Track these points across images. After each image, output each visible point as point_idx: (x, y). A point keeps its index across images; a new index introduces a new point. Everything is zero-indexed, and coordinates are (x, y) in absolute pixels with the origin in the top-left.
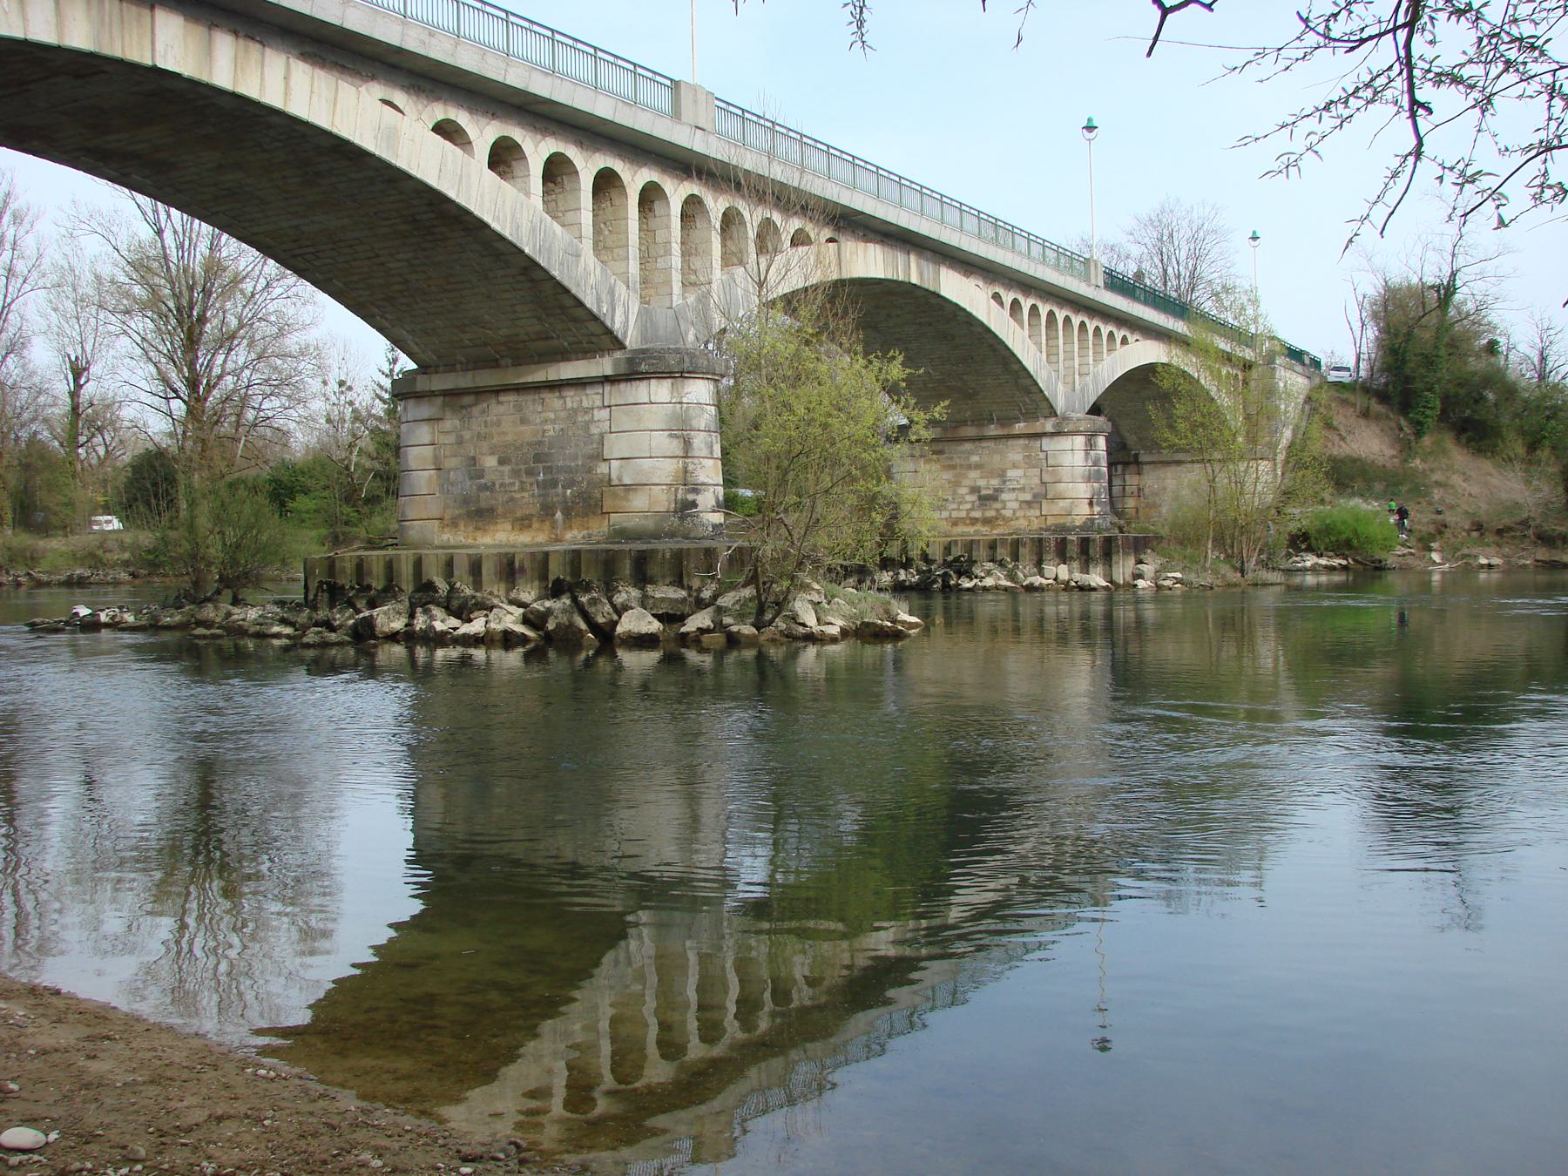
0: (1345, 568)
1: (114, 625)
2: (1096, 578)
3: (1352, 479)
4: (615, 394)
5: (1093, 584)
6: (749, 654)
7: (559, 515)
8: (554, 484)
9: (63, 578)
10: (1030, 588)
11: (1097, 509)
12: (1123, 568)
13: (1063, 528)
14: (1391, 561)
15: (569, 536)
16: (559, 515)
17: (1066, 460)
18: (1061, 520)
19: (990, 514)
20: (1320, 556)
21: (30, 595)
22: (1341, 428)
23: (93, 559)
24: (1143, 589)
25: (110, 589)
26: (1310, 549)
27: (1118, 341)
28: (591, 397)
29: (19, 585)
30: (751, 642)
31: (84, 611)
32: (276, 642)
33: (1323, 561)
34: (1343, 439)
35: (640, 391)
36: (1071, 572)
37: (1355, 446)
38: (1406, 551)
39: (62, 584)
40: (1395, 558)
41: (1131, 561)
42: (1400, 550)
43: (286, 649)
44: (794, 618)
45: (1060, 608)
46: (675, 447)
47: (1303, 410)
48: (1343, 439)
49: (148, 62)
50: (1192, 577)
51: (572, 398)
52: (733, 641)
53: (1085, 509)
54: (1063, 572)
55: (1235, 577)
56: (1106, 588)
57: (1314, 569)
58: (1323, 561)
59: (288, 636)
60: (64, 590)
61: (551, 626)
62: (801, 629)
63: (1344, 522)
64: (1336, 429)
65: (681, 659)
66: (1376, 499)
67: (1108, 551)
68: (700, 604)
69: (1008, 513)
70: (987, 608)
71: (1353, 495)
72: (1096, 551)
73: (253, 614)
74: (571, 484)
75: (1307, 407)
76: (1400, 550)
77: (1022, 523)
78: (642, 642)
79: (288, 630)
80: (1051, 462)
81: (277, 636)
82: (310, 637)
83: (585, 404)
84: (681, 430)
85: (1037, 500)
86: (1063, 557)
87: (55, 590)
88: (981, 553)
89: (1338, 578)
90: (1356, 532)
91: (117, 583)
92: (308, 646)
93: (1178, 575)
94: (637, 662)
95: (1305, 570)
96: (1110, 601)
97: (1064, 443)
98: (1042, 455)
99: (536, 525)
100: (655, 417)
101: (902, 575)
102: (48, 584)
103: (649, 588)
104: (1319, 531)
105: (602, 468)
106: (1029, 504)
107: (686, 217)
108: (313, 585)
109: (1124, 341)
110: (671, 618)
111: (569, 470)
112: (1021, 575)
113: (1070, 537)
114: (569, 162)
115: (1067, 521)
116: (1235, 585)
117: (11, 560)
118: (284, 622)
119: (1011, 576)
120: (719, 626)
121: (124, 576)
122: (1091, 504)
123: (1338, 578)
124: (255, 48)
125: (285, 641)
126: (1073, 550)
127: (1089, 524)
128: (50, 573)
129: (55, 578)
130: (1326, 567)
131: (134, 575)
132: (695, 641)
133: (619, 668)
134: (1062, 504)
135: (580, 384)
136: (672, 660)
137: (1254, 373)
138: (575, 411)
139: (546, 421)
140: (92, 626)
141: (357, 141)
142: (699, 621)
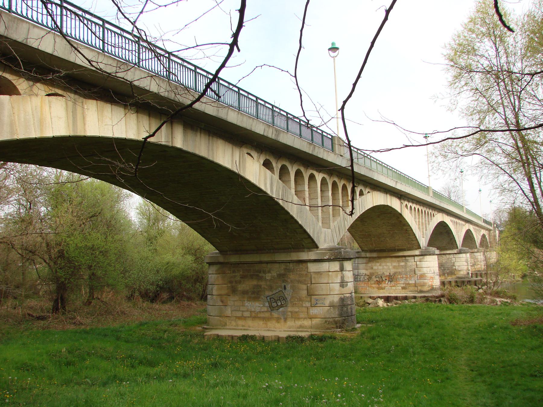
4: (456, 256)
7: (446, 275)
8: (445, 270)
15: (448, 278)
16: (446, 275)
17: (479, 257)
18: (479, 269)
28: (452, 256)
35: (461, 255)
46: (466, 264)
49: (386, 204)
51: (448, 256)
74: (448, 270)
80: (476, 258)
83: (450, 257)
84: (467, 261)
97: (478, 254)
98: (474, 256)
99: (442, 276)
100: (463, 259)
105: (454, 267)
107: (322, 184)
109: (361, 194)
111: (448, 268)
114: (301, 173)
115: (480, 269)
124: (80, 99)
135: (450, 254)
138: (448, 258)
139: (443, 260)
141: (396, 209)
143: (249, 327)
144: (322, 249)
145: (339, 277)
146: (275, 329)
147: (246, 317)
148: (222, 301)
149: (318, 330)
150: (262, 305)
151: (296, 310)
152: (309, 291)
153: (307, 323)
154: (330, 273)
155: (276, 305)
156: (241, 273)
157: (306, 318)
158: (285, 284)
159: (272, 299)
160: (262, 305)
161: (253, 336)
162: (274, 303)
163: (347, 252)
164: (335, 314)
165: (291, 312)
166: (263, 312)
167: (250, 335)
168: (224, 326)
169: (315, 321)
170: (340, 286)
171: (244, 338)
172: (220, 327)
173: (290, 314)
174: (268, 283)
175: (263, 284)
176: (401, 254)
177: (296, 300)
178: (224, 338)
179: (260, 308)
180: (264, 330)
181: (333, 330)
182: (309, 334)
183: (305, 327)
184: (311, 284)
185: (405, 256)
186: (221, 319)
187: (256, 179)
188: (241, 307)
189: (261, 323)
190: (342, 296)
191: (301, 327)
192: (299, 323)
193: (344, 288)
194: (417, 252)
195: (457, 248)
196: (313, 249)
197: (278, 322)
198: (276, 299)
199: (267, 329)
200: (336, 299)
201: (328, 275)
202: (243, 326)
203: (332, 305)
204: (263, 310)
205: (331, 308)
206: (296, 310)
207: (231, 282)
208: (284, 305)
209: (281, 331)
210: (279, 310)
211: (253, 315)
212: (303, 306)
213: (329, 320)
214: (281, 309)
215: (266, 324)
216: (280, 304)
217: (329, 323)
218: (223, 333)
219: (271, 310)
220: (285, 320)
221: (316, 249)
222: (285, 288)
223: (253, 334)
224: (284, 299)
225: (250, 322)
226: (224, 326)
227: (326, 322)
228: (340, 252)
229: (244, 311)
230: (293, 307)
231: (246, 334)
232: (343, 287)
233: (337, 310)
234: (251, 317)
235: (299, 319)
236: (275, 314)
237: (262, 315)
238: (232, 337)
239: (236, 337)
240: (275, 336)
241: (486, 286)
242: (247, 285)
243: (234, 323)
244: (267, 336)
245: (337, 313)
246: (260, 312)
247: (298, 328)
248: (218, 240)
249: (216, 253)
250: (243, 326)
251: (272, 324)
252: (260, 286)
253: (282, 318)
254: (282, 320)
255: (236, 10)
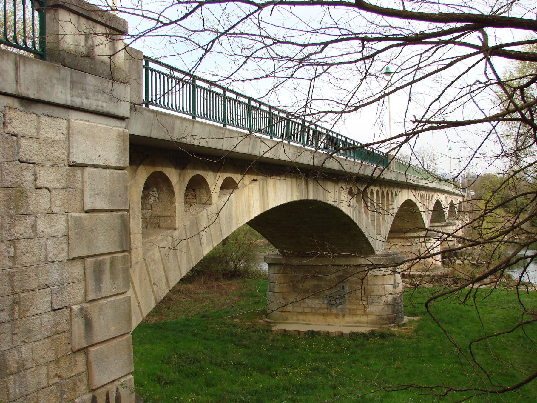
135: (438, 226)
143: (310, 321)
144: (378, 256)
145: (392, 280)
146: (334, 324)
147: (306, 313)
148: (284, 298)
149: (375, 326)
150: (322, 303)
151: (354, 307)
152: (366, 292)
153: (364, 319)
154: (385, 276)
155: (335, 303)
156: (302, 273)
157: (363, 315)
158: (344, 285)
159: (331, 298)
160: (322, 303)
161: (319, 332)
162: (333, 301)
163: (399, 258)
164: (388, 312)
165: (349, 309)
166: (323, 308)
167: (315, 330)
168: (286, 320)
169: (371, 318)
170: (393, 287)
171: (311, 334)
172: (282, 321)
173: (347, 310)
174: (328, 283)
175: (322, 283)
176: (407, 235)
177: (354, 299)
178: (291, 333)
179: (319, 305)
180: (325, 325)
181: (387, 325)
182: (369, 329)
183: (362, 323)
184: (368, 285)
185: (411, 237)
186: (283, 314)
187: (350, 212)
188: (302, 304)
189: (321, 318)
190: (395, 296)
191: (358, 322)
192: (356, 319)
193: (396, 289)
194: (423, 234)
195: (445, 221)
196: (370, 255)
197: (337, 318)
198: (335, 297)
199: (327, 324)
200: (390, 298)
201: (383, 278)
202: (304, 320)
203: (386, 304)
204: (322, 307)
205: (385, 307)
206: (354, 307)
207: (292, 281)
208: (343, 303)
209: (340, 326)
210: (338, 307)
211: (314, 310)
212: (360, 305)
213: (383, 316)
214: (340, 307)
215: (326, 319)
216: (338, 302)
217: (384, 319)
218: (290, 328)
219: (331, 307)
220: (344, 316)
221: (372, 255)
222: (343, 288)
223: (318, 330)
224: (342, 298)
225: (310, 317)
226: (285, 320)
227: (381, 318)
228: (394, 258)
229: (305, 307)
230: (351, 304)
231: (311, 329)
232: (395, 288)
233: (390, 308)
234: (311, 312)
235: (356, 315)
236: (334, 311)
237: (322, 311)
238: (299, 332)
239: (303, 333)
240: (338, 332)
241: (471, 257)
242: (309, 284)
243: (295, 318)
244: (332, 332)
245: (390, 311)
246: (320, 308)
247: (355, 323)
248: (284, 245)
249: (278, 255)
250: (304, 320)
251: (331, 319)
252: (320, 286)
253: (341, 314)
254: (341, 316)
255: (414, 115)
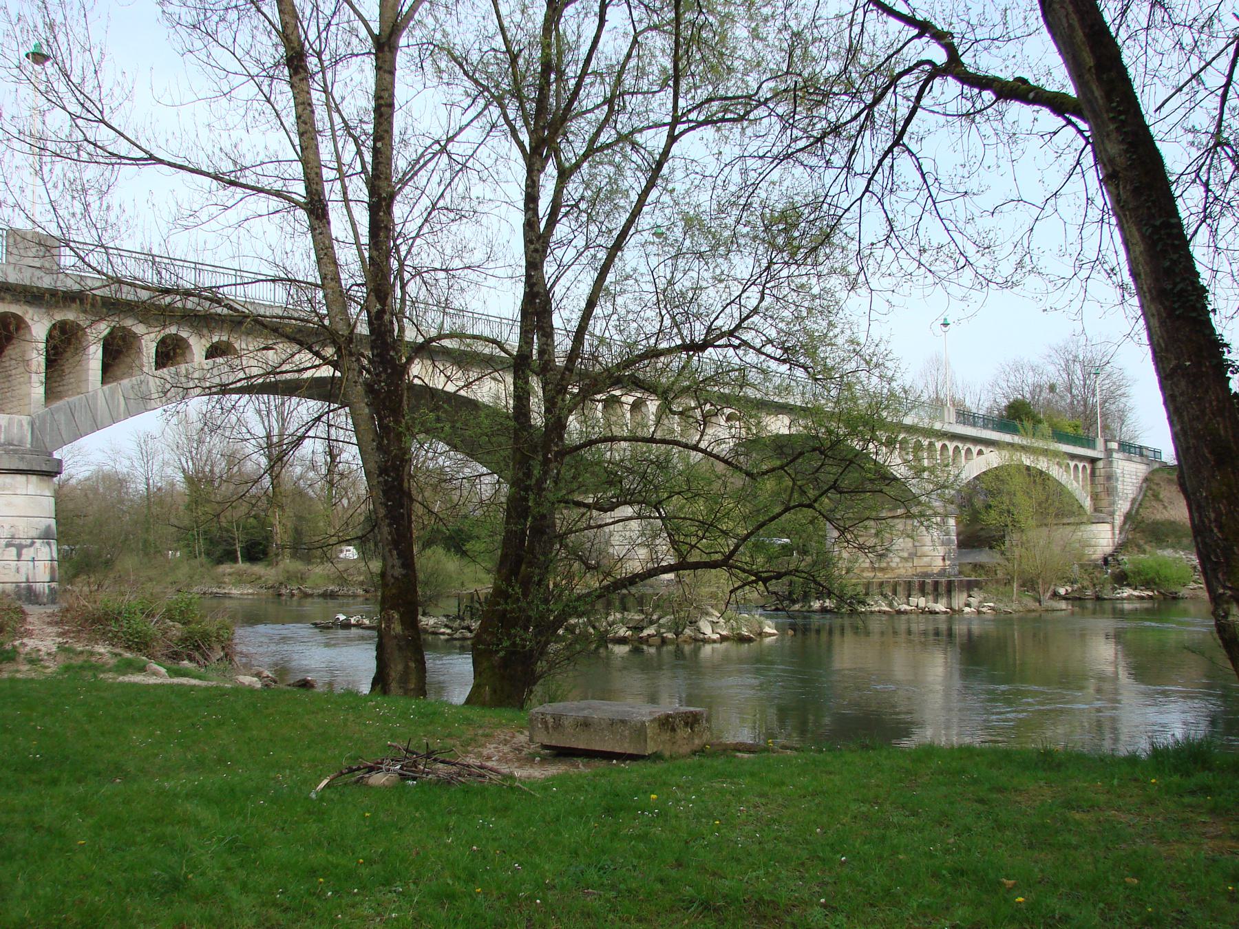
0: (1151, 597)
1: (359, 625)
2: (940, 607)
3: (1167, 536)
5: (937, 610)
6: (671, 648)
9: (321, 591)
10: (899, 612)
11: (948, 563)
12: (959, 600)
13: (926, 575)
14: (1183, 592)
18: (925, 570)
19: (884, 565)
20: (1136, 589)
21: (300, 604)
22: (1165, 500)
23: (342, 579)
24: (967, 613)
25: (351, 600)
26: (1128, 585)
27: (963, 452)
29: (293, 595)
30: (672, 642)
31: (342, 617)
32: (442, 637)
33: (1136, 593)
34: (1165, 507)
36: (927, 602)
37: (1172, 513)
38: (1196, 586)
39: (320, 596)
40: (1188, 592)
41: (965, 595)
42: (1192, 585)
43: (447, 640)
44: (698, 630)
45: (919, 625)
47: (1141, 488)
48: (1165, 507)
50: (1001, 606)
52: (664, 641)
53: (940, 563)
54: (922, 602)
55: (1033, 605)
56: (946, 613)
57: (1129, 598)
58: (1136, 593)
59: (448, 634)
60: (321, 600)
61: (577, 631)
62: (701, 636)
63: (1151, 567)
64: (1161, 501)
65: (642, 651)
66: (1183, 550)
67: (950, 589)
68: (651, 623)
69: (893, 565)
70: (875, 625)
71: (1167, 547)
72: (942, 589)
73: (432, 621)
75: (1144, 485)
76: (1192, 585)
77: (902, 571)
78: (622, 641)
79: (449, 631)
81: (443, 634)
82: (457, 635)
85: (913, 555)
86: (923, 592)
87: (316, 600)
88: (874, 589)
89: (1146, 605)
90: (1158, 573)
91: (355, 596)
92: (456, 639)
93: (991, 604)
94: (621, 650)
95: (1122, 599)
96: (950, 620)
101: (827, 603)
102: (311, 595)
103: (626, 613)
104: (1134, 573)
106: (906, 559)
108: (462, 607)
110: (638, 628)
112: (895, 604)
113: (927, 581)
115: (929, 570)
116: (1034, 611)
117: (288, 579)
118: (446, 626)
119: (890, 605)
120: (658, 634)
121: (360, 592)
122: (944, 560)
123: (1146, 605)
125: (446, 637)
126: (929, 588)
127: (943, 572)
128: (313, 588)
129: (316, 591)
130: (1138, 597)
131: (366, 591)
132: (645, 641)
133: (612, 652)
134: (925, 559)
136: (636, 651)
137: (1100, 464)
140: (346, 626)
142: (651, 631)
